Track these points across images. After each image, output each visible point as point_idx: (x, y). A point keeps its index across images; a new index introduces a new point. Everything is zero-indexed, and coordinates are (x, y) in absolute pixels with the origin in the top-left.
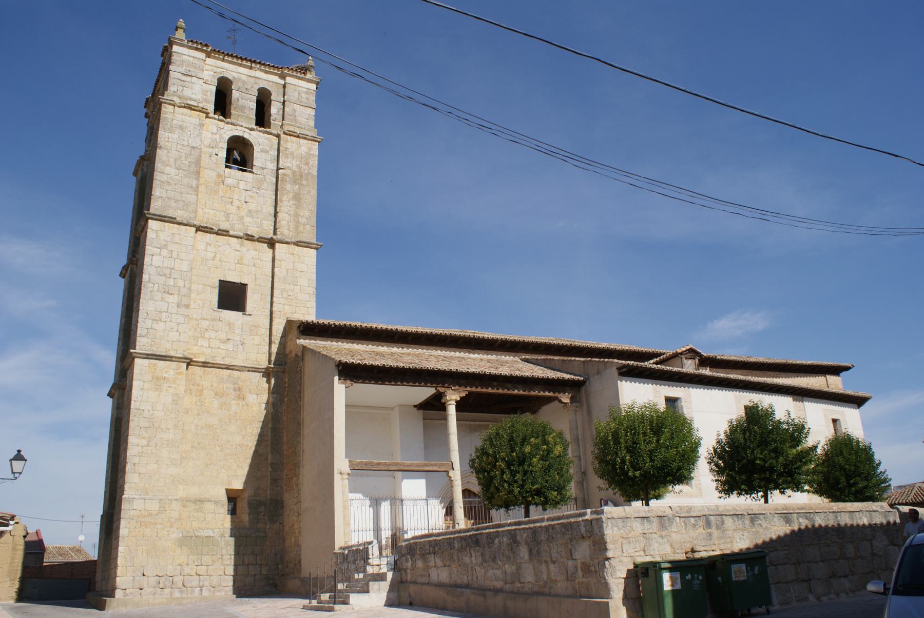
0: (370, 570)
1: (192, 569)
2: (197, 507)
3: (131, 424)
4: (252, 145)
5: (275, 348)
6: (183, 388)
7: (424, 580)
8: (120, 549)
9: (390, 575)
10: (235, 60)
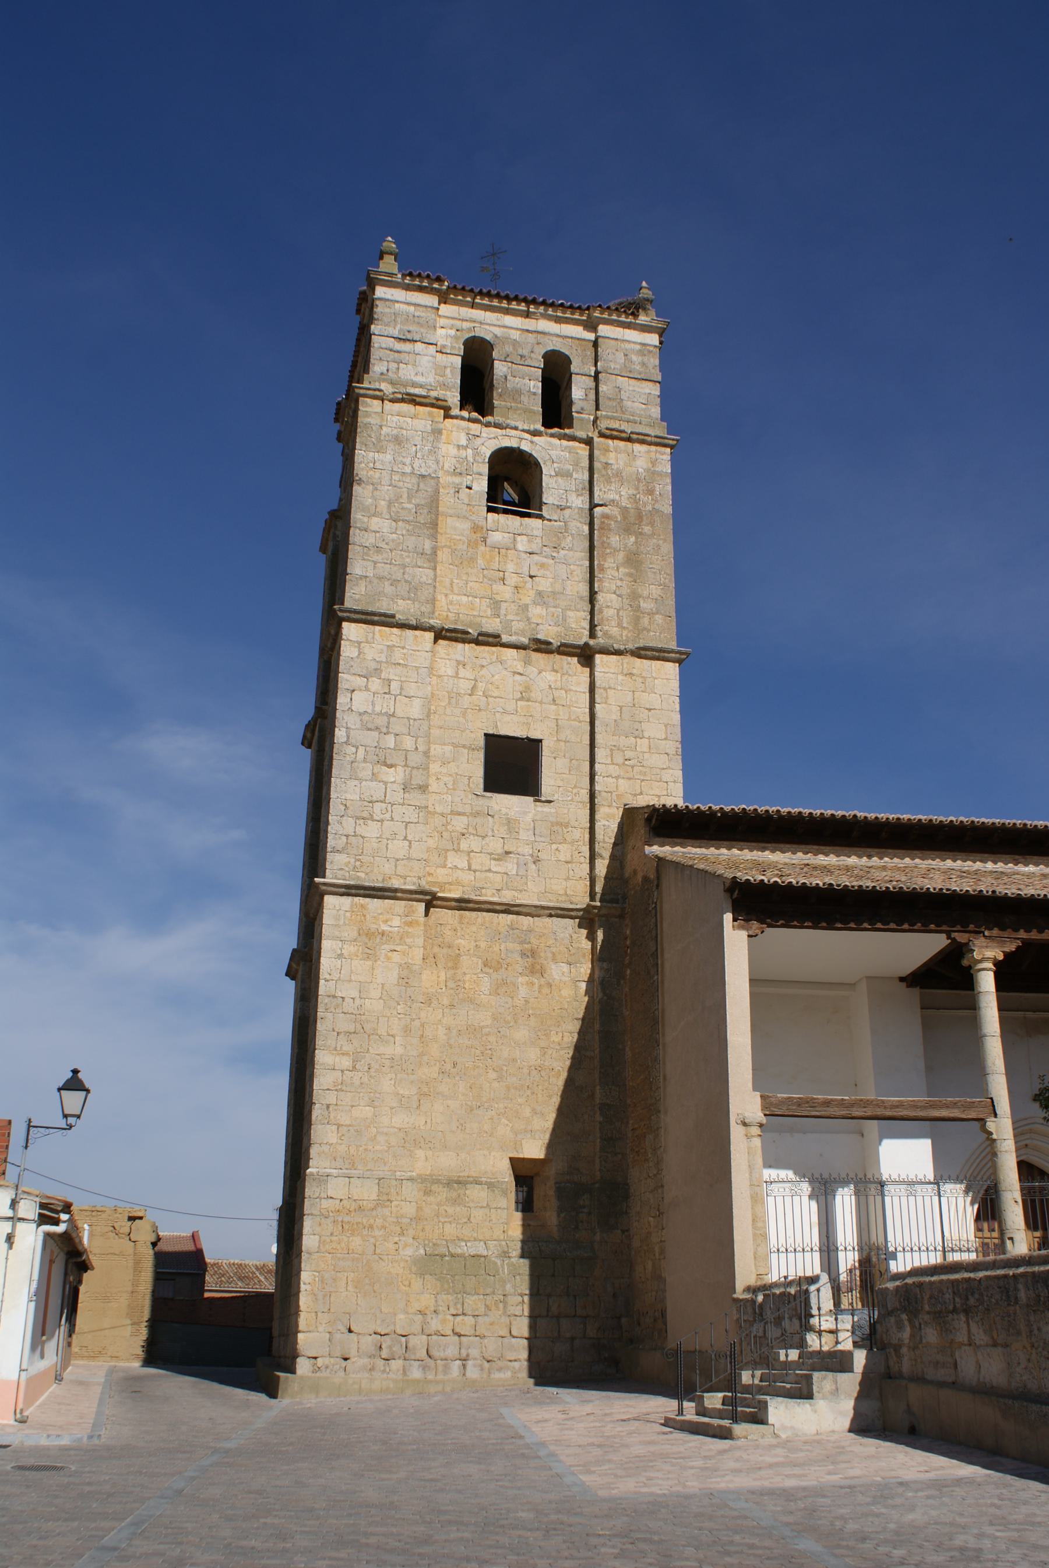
0: (813, 1342)
1: (444, 1321)
2: (454, 1194)
3: (320, 1026)
4: (537, 465)
5: (602, 867)
6: (418, 954)
7: (943, 1374)
8: (305, 1276)
9: (860, 1358)
10: (495, 303)
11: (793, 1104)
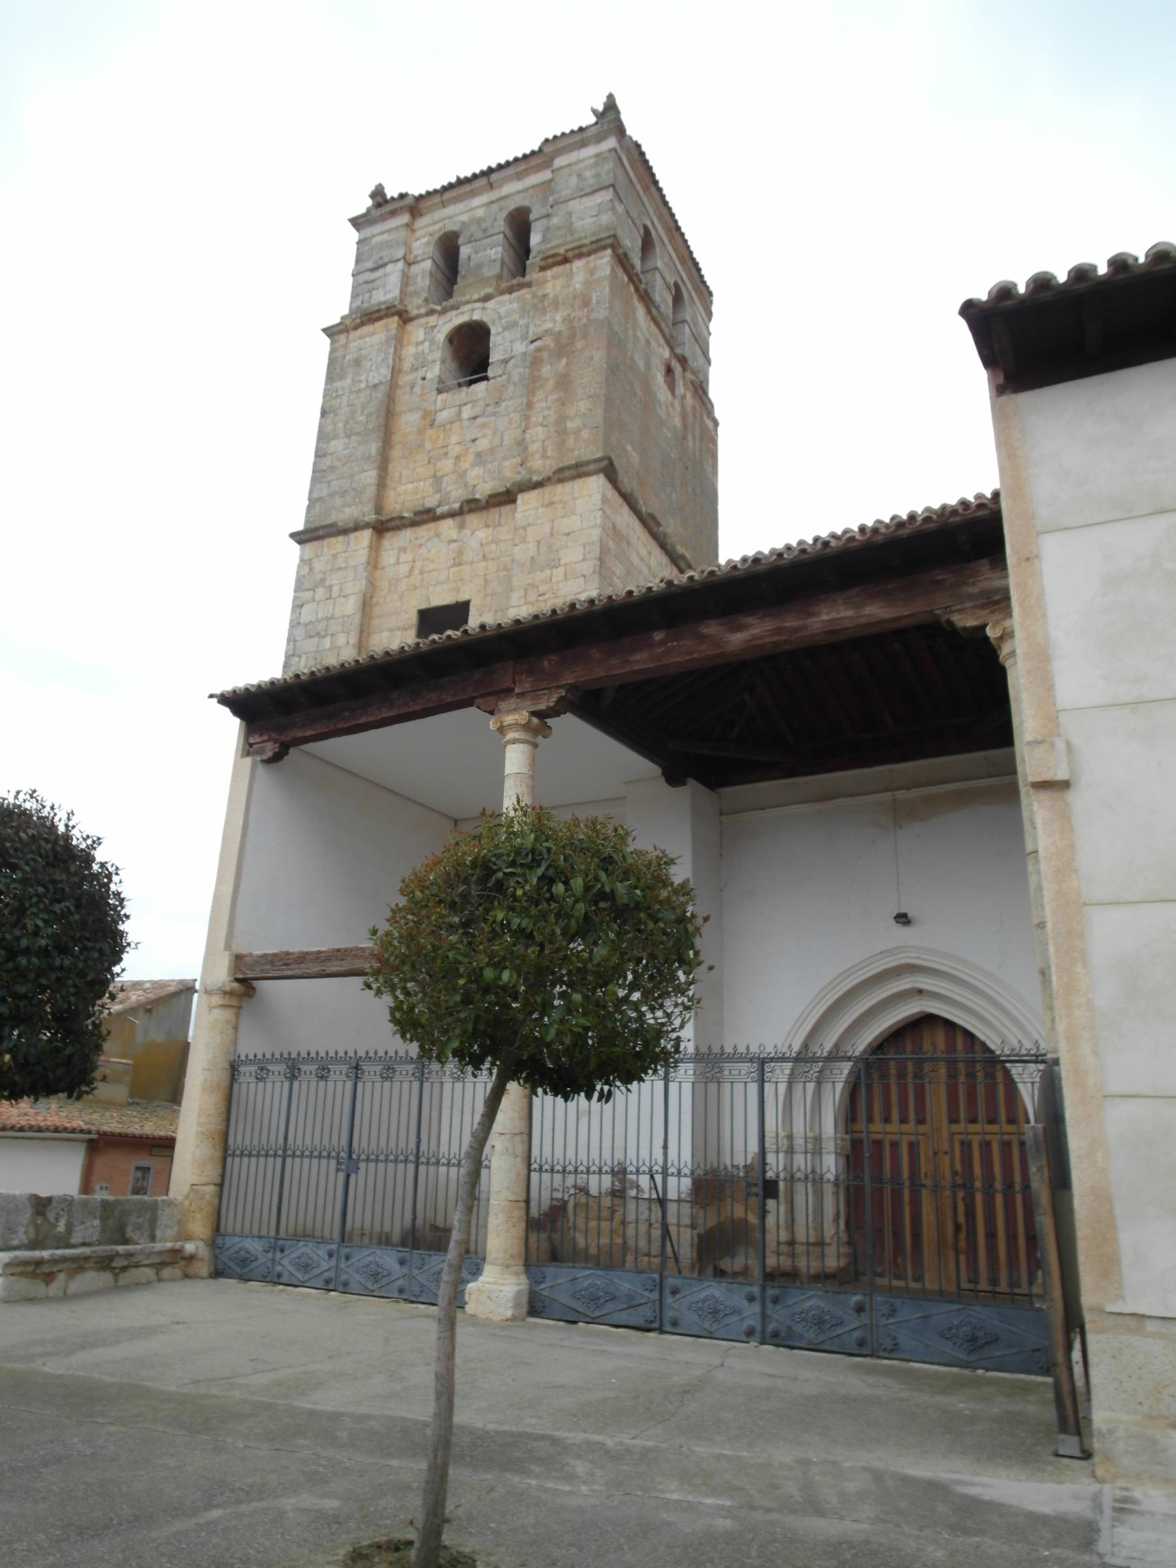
11: (267, 963)
